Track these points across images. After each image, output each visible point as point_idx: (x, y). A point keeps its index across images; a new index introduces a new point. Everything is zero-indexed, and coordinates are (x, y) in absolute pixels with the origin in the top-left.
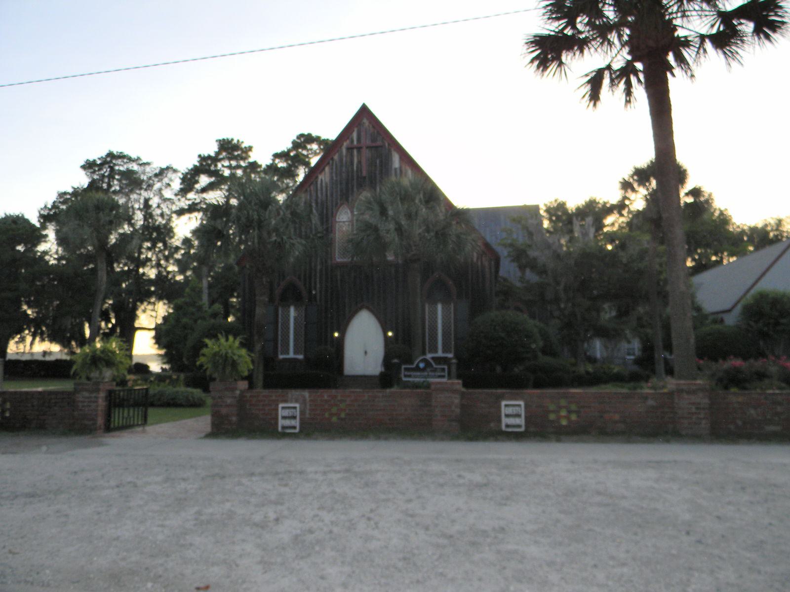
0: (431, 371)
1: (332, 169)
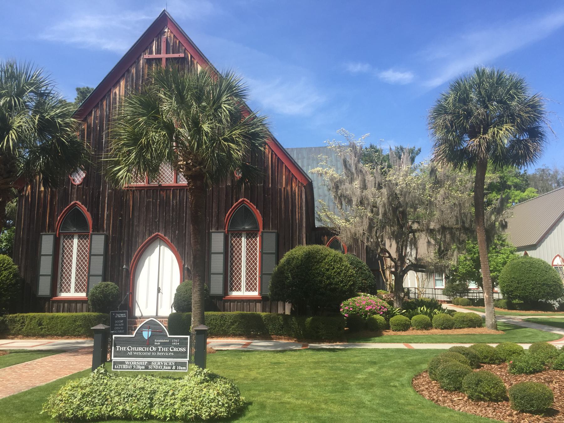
0: (163, 345)
1: (126, 82)
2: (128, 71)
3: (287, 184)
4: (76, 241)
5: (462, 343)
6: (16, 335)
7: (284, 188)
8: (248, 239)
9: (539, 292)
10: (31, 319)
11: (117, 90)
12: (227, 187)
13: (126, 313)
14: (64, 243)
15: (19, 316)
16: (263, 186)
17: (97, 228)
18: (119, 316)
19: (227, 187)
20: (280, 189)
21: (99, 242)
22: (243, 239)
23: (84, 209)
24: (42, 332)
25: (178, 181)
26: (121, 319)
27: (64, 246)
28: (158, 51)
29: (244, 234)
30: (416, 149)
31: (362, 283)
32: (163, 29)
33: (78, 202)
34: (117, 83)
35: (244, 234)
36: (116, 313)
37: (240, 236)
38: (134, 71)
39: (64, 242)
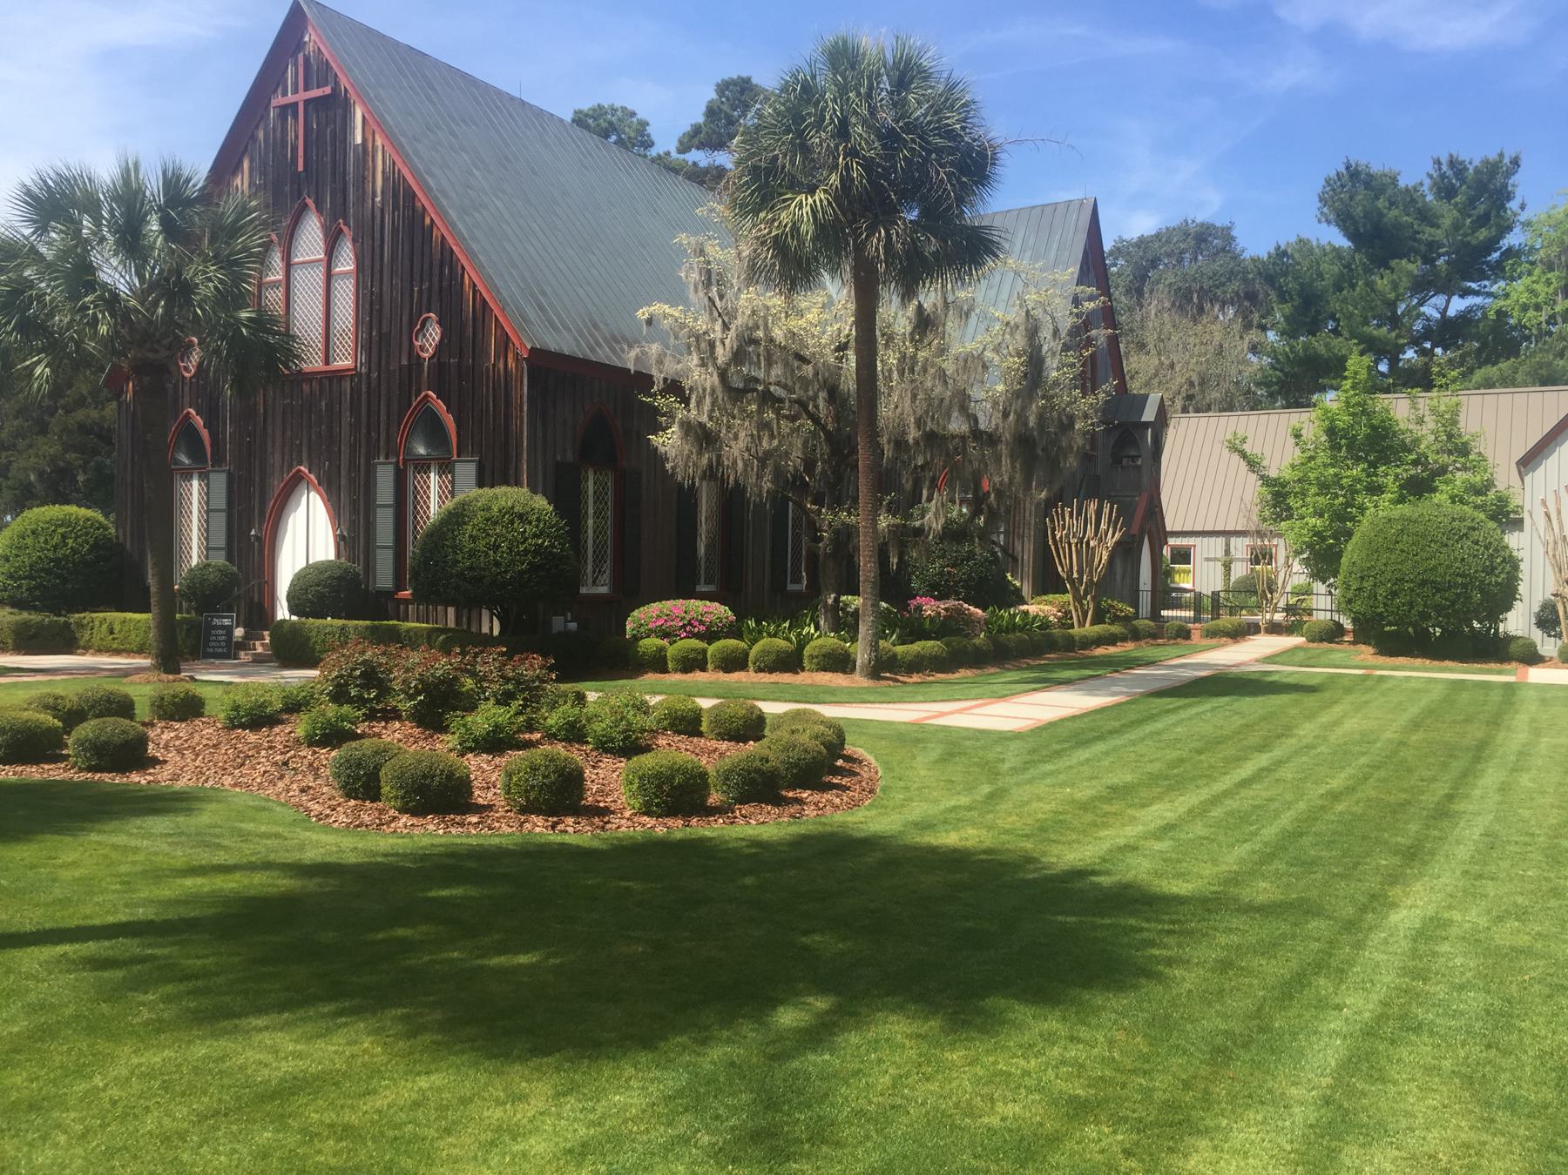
1: (251, 161)
2: (253, 137)
3: (497, 357)
4: (195, 483)
5: (809, 703)
6: (86, 649)
7: (494, 365)
8: (440, 477)
9: (1411, 604)
10: (101, 623)
11: (238, 181)
12: (401, 367)
13: (232, 617)
14: (414, 479)
15: (87, 616)
16: (459, 363)
17: (218, 460)
18: (216, 622)
19: (401, 367)
20: (488, 368)
21: (219, 480)
22: (432, 475)
23: (199, 421)
24: (114, 646)
25: (331, 359)
26: (223, 627)
27: (415, 487)
28: (295, 91)
29: (196, 476)
30: (1506, 160)
31: (941, 574)
32: (302, 36)
33: (430, 393)
34: (237, 167)
35: (196, 476)
36: (213, 617)
37: (427, 470)
38: (261, 135)
39: (415, 478)
